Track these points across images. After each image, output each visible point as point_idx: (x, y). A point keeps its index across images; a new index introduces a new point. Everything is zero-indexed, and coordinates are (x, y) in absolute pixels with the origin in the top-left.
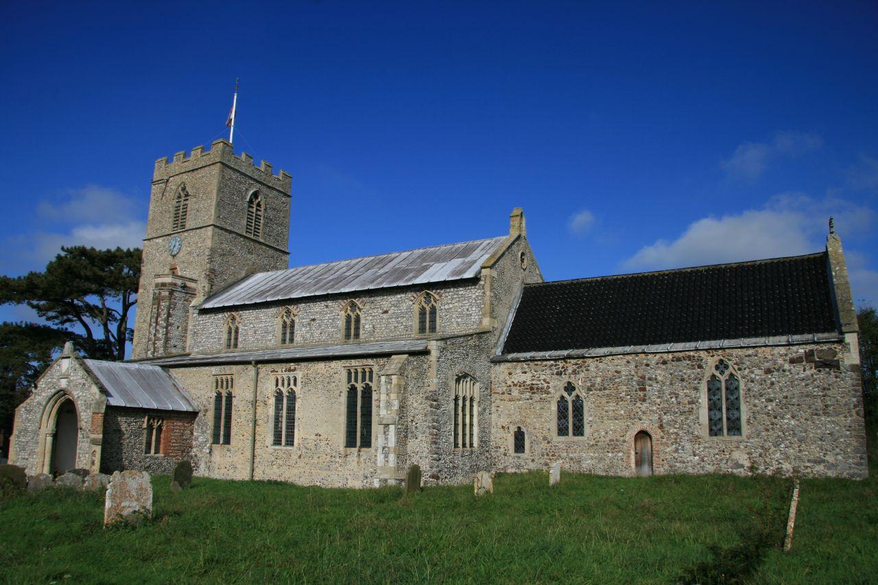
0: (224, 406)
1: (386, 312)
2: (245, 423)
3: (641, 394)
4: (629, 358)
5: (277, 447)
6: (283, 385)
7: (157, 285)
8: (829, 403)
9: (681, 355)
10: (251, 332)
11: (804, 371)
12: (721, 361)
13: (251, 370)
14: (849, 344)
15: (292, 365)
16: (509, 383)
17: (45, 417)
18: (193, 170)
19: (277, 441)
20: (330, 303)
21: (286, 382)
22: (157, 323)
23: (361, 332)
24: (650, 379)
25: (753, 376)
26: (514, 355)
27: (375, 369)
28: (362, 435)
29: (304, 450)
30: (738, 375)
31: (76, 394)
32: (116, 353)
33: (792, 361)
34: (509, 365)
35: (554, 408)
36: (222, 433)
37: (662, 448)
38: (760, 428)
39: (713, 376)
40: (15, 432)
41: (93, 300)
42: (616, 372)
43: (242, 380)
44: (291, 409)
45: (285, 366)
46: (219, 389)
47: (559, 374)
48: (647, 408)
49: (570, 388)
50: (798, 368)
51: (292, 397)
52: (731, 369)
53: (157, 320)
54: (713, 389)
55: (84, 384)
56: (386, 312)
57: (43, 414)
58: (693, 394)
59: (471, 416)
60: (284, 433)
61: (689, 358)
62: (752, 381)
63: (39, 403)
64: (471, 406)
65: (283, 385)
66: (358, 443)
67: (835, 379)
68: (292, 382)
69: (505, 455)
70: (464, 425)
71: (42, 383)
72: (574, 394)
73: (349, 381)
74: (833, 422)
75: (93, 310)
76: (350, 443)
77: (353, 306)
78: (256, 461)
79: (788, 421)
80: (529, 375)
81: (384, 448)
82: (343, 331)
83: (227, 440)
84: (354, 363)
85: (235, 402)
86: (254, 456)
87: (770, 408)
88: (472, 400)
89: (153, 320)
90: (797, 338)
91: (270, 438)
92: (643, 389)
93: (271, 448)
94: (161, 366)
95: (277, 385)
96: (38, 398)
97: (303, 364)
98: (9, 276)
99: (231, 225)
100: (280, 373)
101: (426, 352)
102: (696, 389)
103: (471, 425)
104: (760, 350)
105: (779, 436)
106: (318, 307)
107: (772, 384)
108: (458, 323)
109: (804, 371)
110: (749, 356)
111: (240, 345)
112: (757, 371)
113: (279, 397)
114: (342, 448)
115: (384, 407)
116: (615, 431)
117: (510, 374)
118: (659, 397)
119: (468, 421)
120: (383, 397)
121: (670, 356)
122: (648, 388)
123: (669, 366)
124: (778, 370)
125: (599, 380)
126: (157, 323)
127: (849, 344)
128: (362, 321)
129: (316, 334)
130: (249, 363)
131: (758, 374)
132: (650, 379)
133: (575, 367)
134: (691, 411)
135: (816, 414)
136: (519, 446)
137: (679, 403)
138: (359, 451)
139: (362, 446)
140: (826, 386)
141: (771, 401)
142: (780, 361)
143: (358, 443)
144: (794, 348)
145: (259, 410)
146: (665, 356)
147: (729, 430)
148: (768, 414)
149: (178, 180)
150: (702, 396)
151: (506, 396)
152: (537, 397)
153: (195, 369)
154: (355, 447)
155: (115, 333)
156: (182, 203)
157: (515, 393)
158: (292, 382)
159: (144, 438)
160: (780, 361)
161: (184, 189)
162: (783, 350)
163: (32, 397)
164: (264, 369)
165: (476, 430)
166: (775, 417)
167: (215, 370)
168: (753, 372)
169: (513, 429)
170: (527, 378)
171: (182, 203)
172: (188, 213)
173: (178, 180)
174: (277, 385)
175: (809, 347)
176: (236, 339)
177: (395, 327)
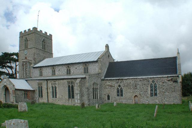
1: (76, 68)
4: (132, 79)
7: (23, 62)
15: (55, 81)
19: (53, 97)
30: (157, 83)
31: (8, 86)
41: (9, 64)
44: (56, 90)
49: (119, 86)
50: (169, 82)
56: (76, 68)
60: (54, 94)
64: (97, 90)
68: (55, 84)
70: (95, 94)
75: (8, 67)
76: (69, 97)
77: (86, 65)
83: (42, 97)
84: (69, 80)
88: (97, 88)
91: (52, 96)
102: (148, 87)
103: (97, 94)
106: (60, 67)
107: (164, 85)
113: (53, 88)
131: (161, 84)
136: (109, 99)
149: (25, 37)
152: (112, 88)
158: (55, 84)
162: (166, 78)
165: (98, 95)
169: (107, 95)
170: (110, 84)
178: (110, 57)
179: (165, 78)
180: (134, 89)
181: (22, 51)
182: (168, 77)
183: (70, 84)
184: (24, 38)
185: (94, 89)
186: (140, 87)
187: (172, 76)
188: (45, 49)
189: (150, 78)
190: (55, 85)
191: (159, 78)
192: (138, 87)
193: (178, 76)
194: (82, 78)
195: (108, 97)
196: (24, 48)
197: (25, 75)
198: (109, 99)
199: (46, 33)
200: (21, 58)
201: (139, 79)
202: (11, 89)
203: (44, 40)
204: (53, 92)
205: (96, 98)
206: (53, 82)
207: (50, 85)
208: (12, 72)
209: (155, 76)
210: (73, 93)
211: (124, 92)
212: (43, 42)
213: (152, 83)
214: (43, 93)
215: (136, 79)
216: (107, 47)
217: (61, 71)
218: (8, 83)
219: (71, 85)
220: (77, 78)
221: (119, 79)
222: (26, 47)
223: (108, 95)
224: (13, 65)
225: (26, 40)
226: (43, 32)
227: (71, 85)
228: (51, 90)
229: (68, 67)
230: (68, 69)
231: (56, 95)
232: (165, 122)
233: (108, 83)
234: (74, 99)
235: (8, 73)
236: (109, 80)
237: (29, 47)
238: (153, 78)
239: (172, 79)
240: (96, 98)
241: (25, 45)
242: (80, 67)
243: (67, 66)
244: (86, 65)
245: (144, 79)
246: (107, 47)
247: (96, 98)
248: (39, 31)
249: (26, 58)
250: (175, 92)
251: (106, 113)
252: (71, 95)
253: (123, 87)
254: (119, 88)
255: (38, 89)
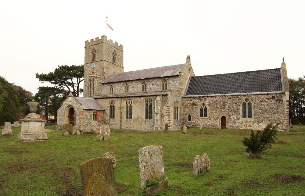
0: (112, 109)
1: (153, 84)
2: (118, 113)
3: (223, 106)
4: (220, 97)
5: (127, 119)
6: (128, 103)
7: (90, 77)
8: (278, 110)
9: (235, 96)
10: (117, 90)
11: (272, 101)
12: (247, 98)
13: (119, 100)
14: (286, 94)
15: (130, 98)
16: (187, 103)
17: (66, 112)
18: (96, 44)
19: (127, 117)
20: (138, 82)
21: (129, 103)
22: (91, 87)
23: (147, 89)
24: (226, 103)
25: (256, 103)
26: (189, 96)
27: (153, 99)
28: (150, 116)
29: (135, 120)
30: (252, 102)
31: (74, 106)
32: (77, 95)
33: (268, 99)
34: (187, 98)
35: (199, 110)
36: (112, 116)
37: (229, 121)
38: (258, 116)
39: (244, 102)
40: (58, 116)
41: (69, 81)
42: (217, 101)
43: (117, 102)
44: (131, 109)
45: (128, 98)
46: (111, 104)
47: (201, 101)
48: (225, 110)
49: (203, 105)
50: (270, 101)
51: (131, 106)
52: (249, 101)
53: (93, 84)
54: (244, 105)
55: (76, 103)
56: (153, 84)
57: (65, 111)
58: (238, 107)
59: (178, 111)
60: (129, 114)
61: (238, 97)
62: (256, 104)
63: (64, 109)
64: (178, 109)
65: (128, 103)
66: (149, 118)
67: (281, 104)
68: (127, 103)
69: (186, 122)
70: (176, 114)
71: (64, 103)
72: (205, 106)
73: (146, 102)
74: (279, 116)
75: (69, 84)
76: (147, 118)
77: (165, 80)
78: (122, 123)
79: (266, 115)
80: (192, 101)
81: (156, 119)
82: (142, 89)
83: (114, 117)
84: (147, 98)
85: (115, 108)
86: (121, 121)
87: (261, 111)
88: (178, 107)
89: (90, 86)
90: (270, 92)
91: (125, 117)
92: (224, 105)
93: (126, 120)
94: (94, 98)
95: (126, 103)
96: (63, 107)
97: (133, 98)
98: (44, 74)
99: (108, 60)
100: (127, 100)
101: (167, 95)
102: (239, 106)
103: (178, 114)
104: (259, 96)
105: (263, 119)
106: (135, 83)
107: (262, 105)
108: (173, 87)
109: (272, 101)
110: (255, 97)
111: (114, 93)
112: (257, 101)
113: (127, 106)
114: (145, 119)
115: (157, 108)
116: (216, 116)
117: (187, 101)
118: (228, 108)
119: (177, 113)
120: (156, 106)
121: (232, 97)
122: (225, 105)
123: (232, 99)
124: (264, 101)
125: (212, 103)
126: (91, 87)
127: (286, 94)
128: (147, 87)
129: (135, 90)
130: (119, 97)
131: (258, 102)
132: (226, 103)
133: (205, 99)
134: (237, 112)
135: (275, 113)
136: (190, 119)
137: (234, 109)
138: (149, 120)
139: (150, 119)
140: (278, 106)
141: (261, 109)
142: (265, 99)
143: (149, 118)
144: (269, 95)
145: (122, 109)
146: (230, 97)
147: (248, 117)
148: (260, 113)
149: (92, 47)
150: (241, 108)
151: (186, 107)
152: (194, 107)
153: (104, 99)
154: (148, 119)
155: (76, 89)
156: (94, 54)
157: (189, 105)
158: (127, 103)
159: (92, 117)
160: (265, 99)
161: (94, 49)
162: (266, 96)
163: (61, 107)
164: (123, 100)
165: (179, 115)
166: (262, 114)
167: (109, 100)
168: (256, 102)
169: (188, 115)
170: (192, 102)
171: (94, 54)
172: (96, 57)
173: (92, 47)
174: (126, 103)
175: (274, 95)
176: (113, 91)
177: (156, 88)
178: (191, 70)
179: (263, 96)
180: (221, 108)
181: (89, 64)
182: (268, 94)
183: (148, 102)
184: (91, 48)
185: (177, 108)
186: (229, 107)
187: (275, 94)
188: (115, 62)
189: (243, 95)
190: (111, 104)
191: (255, 95)
192: (227, 106)
193: (284, 93)
194: (163, 95)
195: (190, 117)
196: (90, 60)
197: (92, 92)
198: (190, 119)
199: (116, 43)
200: (86, 73)
201: (228, 96)
202: (78, 109)
203: (114, 51)
204: (127, 112)
205: (177, 118)
206: (128, 100)
207: (124, 104)
208: (74, 89)
209: (249, 93)
210: (151, 113)
211: (208, 113)
212: (113, 53)
213: (245, 102)
214: (115, 113)
215: (224, 96)
216: (188, 58)
217: (136, 88)
218: (74, 102)
219: (149, 104)
220: (156, 96)
221: (202, 97)
222: (94, 60)
223: (190, 115)
224: (75, 80)
225: (94, 51)
226: (114, 42)
227: (149, 104)
228: (125, 110)
229: (127, 84)
230: (163, 83)
231: (131, 116)
232: (133, 144)
233: (190, 101)
234: (153, 120)
235: (68, 90)
236: (191, 97)
237: (97, 60)
238: (248, 95)
239: (274, 98)
240: (176, 119)
241: (93, 57)
242: (158, 83)
243: (142, 82)
244: (165, 80)
245: (234, 97)
246: (188, 58)
247: (177, 118)
248: (109, 40)
249: (93, 73)
250: (277, 113)
251: (298, 132)
252: (149, 114)
253: (208, 107)
254: (247, 103)
255: (108, 109)
